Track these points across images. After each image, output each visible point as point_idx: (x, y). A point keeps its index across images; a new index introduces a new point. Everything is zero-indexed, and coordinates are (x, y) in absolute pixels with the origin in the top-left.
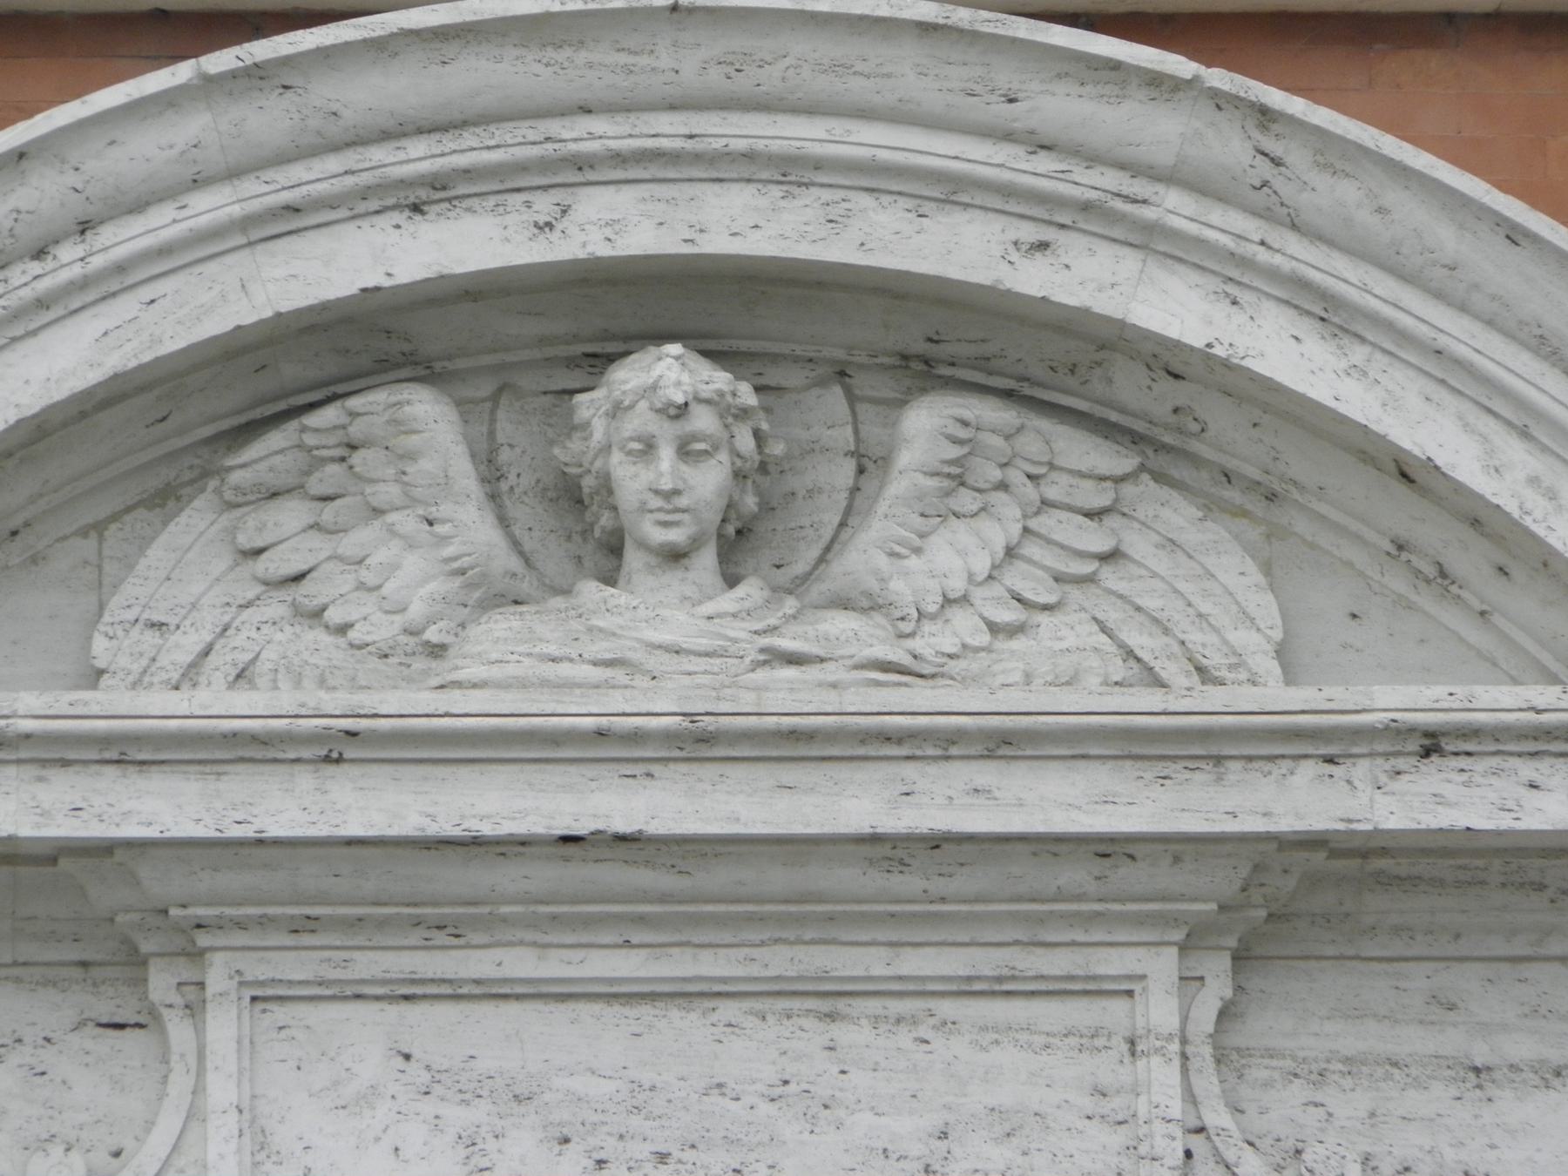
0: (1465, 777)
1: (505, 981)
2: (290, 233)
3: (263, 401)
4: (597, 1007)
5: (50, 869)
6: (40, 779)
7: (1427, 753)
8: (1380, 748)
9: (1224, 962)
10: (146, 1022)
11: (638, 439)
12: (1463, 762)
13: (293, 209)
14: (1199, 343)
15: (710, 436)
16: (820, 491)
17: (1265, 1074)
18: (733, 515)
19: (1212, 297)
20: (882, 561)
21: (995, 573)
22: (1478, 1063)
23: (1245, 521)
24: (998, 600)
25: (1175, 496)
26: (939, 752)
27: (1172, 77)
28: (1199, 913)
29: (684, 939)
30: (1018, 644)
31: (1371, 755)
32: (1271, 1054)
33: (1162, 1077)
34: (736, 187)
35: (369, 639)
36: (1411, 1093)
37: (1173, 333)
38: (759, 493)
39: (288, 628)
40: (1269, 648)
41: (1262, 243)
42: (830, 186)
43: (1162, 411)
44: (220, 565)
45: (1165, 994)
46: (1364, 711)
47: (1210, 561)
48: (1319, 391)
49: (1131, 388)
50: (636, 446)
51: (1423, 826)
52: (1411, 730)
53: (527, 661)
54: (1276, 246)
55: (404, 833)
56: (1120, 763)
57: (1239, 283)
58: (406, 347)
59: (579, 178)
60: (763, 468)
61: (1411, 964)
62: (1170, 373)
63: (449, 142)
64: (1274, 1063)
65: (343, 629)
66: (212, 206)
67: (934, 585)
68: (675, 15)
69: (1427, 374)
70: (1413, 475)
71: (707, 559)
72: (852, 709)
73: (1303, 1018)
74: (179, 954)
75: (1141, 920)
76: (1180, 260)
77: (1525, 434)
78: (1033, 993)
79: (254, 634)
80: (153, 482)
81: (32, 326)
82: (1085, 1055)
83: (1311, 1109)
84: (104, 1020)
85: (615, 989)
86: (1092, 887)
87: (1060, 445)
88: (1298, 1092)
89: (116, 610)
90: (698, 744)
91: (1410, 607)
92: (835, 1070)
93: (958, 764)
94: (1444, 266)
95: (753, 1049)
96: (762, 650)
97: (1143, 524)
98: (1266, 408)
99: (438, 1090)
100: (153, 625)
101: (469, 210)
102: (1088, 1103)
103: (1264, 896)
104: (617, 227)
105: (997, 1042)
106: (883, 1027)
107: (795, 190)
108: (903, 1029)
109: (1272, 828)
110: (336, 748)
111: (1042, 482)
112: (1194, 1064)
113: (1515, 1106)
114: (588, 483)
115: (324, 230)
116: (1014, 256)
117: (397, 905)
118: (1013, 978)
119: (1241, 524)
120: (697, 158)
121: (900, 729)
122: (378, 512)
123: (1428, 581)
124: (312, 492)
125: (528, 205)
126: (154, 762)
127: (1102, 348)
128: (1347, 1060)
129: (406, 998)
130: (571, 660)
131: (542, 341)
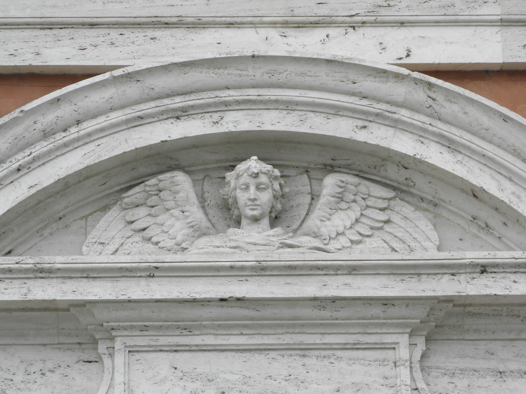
0: (494, 279)
1: (205, 345)
2: (140, 125)
3: (134, 179)
4: (233, 354)
5: (67, 313)
6: (63, 283)
7: (482, 272)
8: (468, 271)
9: (423, 339)
10: (98, 361)
11: (244, 185)
12: (493, 275)
13: (141, 118)
14: (412, 154)
15: (266, 184)
16: (301, 205)
17: (436, 374)
18: (274, 210)
19: (416, 141)
20: (318, 223)
21: (352, 226)
22: (501, 370)
23: (428, 213)
24: (353, 234)
25: (407, 205)
26: (334, 273)
27: (402, 74)
28: (415, 323)
29: (259, 332)
30: (360, 246)
31: (465, 273)
32: (438, 368)
33: (404, 373)
34: (273, 111)
35: (164, 246)
36: (481, 379)
37: (404, 151)
38: (282, 205)
39: (141, 243)
40: (435, 247)
41: (430, 124)
42: (301, 110)
43: (402, 179)
44: (121, 226)
45: (405, 349)
46: (463, 259)
47: (417, 223)
48: (448, 168)
49: (393, 173)
50: (243, 187)
51: (482, 294)
52: (477, 265)
53: (210, 248)
54: (434, 125)
55: (172, 298)
56: (389, 276)
57: (424, 137)
58: (177, 163)
59: (226, 108)
60: (283, 196)
61: (480, 342)
62: (404, 167)
63: (187, 98)
64: (439, 371)
65: (157, 243)
66: (116, 116)
67: (334, 229)
68: (253, 59)
69: (480, 162)
70: (477, 195)
71: (266, 222)
72: (308, 259)
73: (446, 357)
74: (107, 339)
75: (398, 326)
76: (406, 131)
77: (510, 180)
78: (365, 349)
79: (130, 245)
80: (102, 204)
81: (64, 152)
82: (381, 367)
83: (450, 384)
84: (86, 360)
85: (238, 348)
86: (382, 315)
87: (371, 189)
88: (446, 379)
89: (90, 238)
90: (261, 270)
91: (478, 237)
92: (306, 371)
93: (340, 276)
94: (485, 129)
95: (280, 366)
96: (281, 243)
97: (397, 212)
98: (433, 177)
99: (185, 378)
100: (101, 243)
101: (193, 118)
102: (382, 381)
103: (434, 318)
104: (237, 123)
105: (354, 363)
106: (320, 359)
107: (290, 111)
108: (326, 359)
109: (436, 295)
110: (152, 272)
111: (366, 200)
112: (414, 370)
113: (512, 383)
114: (230, 200)
115: (150, 124)
116: (356, 130)
117: (172, 322)
118: (359, 344)
119: (427, 213)
120: (261, 102)
121: (322, 265)
122: (168, 210)
123: (483, 229)
124: (148, 205)
125: (211, 117)
126: (98, 277)
127: (384, 160)
128: (461, 370)
129: (176, 351)
130: (223, 247)
131: (218, 161)
